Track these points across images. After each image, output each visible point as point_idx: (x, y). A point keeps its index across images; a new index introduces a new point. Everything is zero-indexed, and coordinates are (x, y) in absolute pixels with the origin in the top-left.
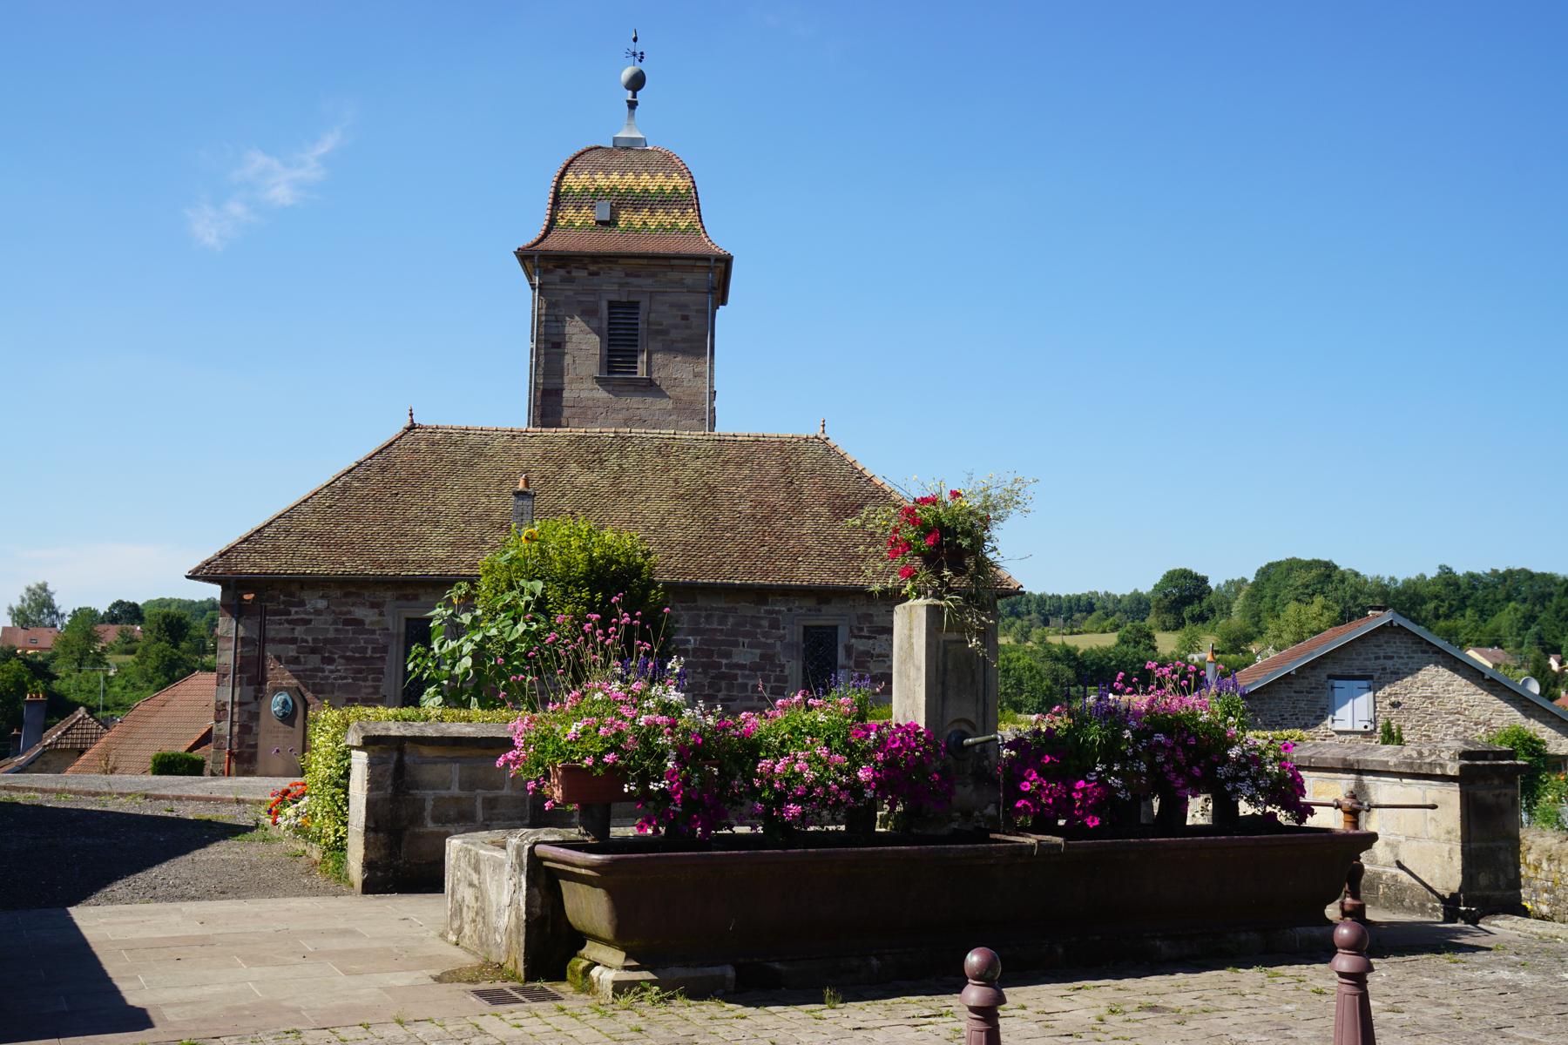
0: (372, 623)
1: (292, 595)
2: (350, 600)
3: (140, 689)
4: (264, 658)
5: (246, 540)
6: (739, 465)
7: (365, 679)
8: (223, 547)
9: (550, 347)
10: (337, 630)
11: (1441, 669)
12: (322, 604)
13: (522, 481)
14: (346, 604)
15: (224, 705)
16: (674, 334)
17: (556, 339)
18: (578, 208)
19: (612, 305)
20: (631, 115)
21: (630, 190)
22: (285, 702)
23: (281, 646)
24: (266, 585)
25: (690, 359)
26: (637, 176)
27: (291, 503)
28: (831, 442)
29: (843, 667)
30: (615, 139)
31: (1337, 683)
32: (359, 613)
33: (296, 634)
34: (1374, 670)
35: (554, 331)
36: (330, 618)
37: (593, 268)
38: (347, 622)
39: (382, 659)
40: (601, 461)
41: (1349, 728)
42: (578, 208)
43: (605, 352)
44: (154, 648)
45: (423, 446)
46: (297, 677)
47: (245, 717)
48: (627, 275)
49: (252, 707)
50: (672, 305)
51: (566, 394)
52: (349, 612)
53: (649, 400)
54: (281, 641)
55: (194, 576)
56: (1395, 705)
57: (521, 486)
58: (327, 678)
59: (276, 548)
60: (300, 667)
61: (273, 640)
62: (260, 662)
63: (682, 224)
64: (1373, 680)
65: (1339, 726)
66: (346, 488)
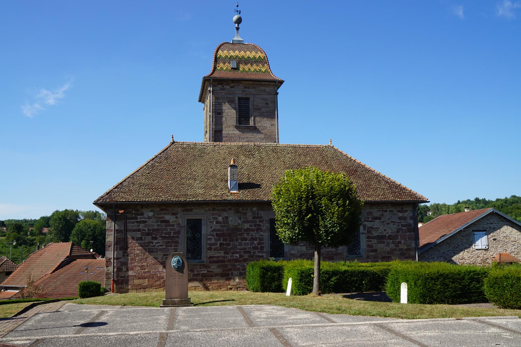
0: (173, 222)
1: (138, 210)
2: (163, 212)
3: (8, 247)
4: (127, 238)
5: (116, 187)
6: (305, 156)
7: (171, 246)
8: (107, 190)
9: (217, 114)
10: (158, 225)
11: (509, 227)
12: (151, 214)
13: (232, 161)
14: (161, 214)
15: (110, 259)
16: (263, 110)
17: (219, 111)
18: (224, 63)
19: (239, 99)
20: (237, 33)
21: (243, 57)
22: (179, 261)
23: (134, 233)
24: (127, 206)
25: (269, 119)
26: (245, 52)
27: (132, 173)
28: (335, 147)
29: (363, 233)
30: (233, 40)
31: (475, 233)
32: (167, 217)
33: (140, 227)
34: (487, 228)
35: (219, 108)
36: (155, 220)
37: (232, 85)
38: (162, 222)
39: (178, 237)
40: (253, 155)
41: (480, 248)
42: (224, 63)
43: (238, 116)
44: (12, 234)
45: (180, 149)
46: (142, 246)
47: (119, 264)
48: (245, 88)
49: (122, 260)
50: (262, 99)
51: (223, 132)
52: (163, 217)
53: (255, 134)
54: (134, 231)
55: (95, 203)
56: (494, 240)
57: (232, 163)
58: (155, 246)
59: (130, 191)
60: (143, 242)
61: (130, 230)
62: (125, 240)
63: (263, 70)
64: (487, 231)
65: (477, 248)
66: (153, 166)
